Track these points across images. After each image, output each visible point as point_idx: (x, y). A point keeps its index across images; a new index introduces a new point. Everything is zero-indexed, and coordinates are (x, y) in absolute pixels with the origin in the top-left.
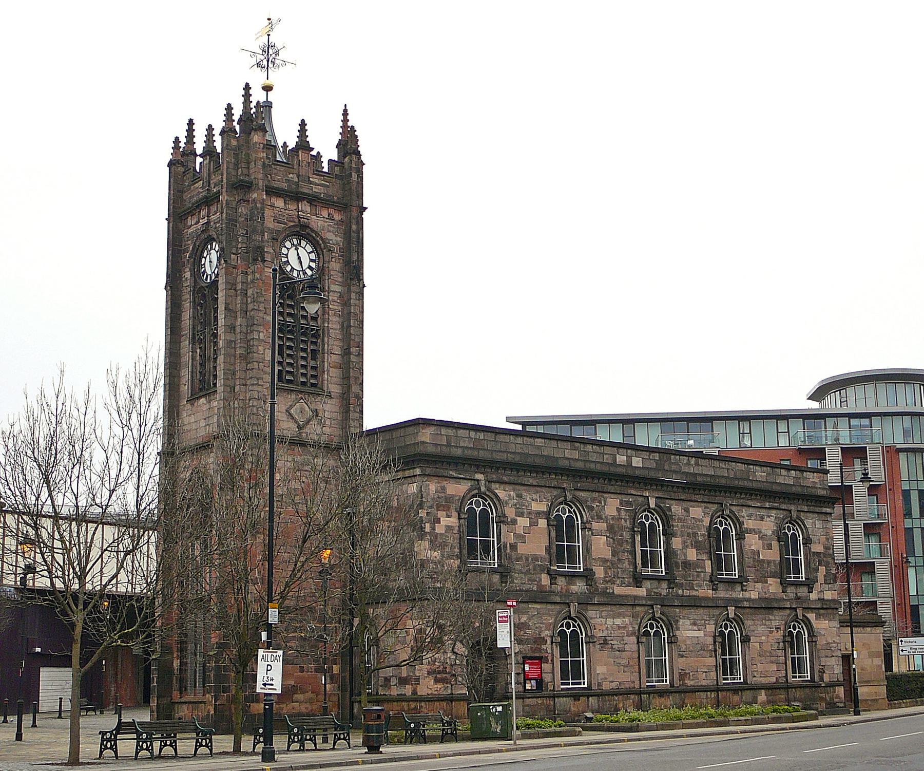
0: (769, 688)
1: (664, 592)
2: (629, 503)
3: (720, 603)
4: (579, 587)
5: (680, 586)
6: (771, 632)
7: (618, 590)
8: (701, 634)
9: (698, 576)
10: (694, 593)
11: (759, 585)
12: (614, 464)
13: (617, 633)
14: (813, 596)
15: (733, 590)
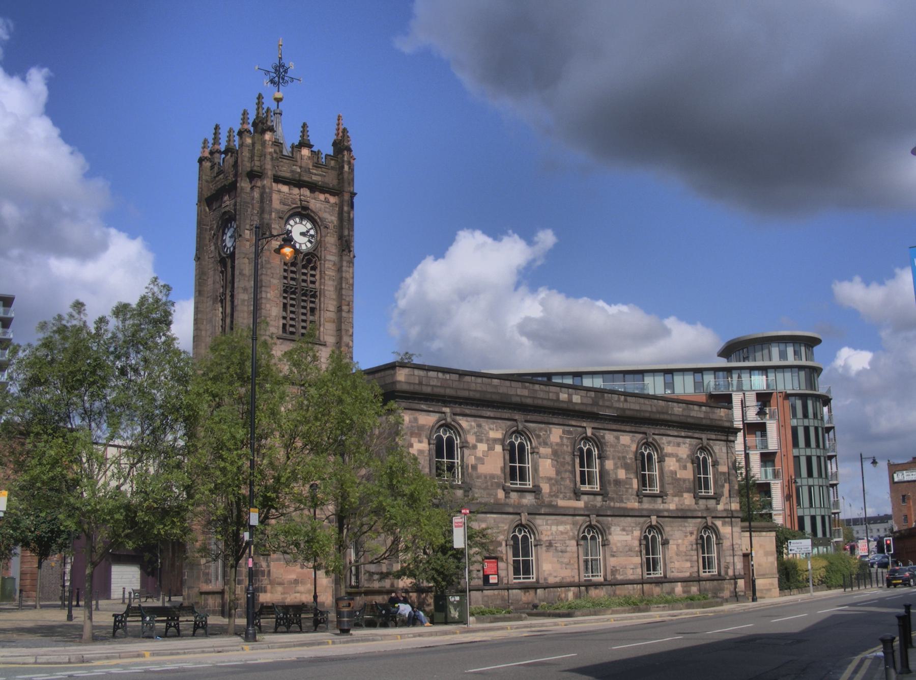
0: (684, 581)
1: (599, 505)
2: (570, 433)
3: (645, 513)
4: (529, 499)
5: (612, 499)
6: (686, 536)
7: (561, 503)
8: (629, 538)
9: (627, 491)
10: (623, 505)
11: (676, 499)
12: (558, 400)
13: (560, 537)
14: (720, 507)
15: (655, 502)
